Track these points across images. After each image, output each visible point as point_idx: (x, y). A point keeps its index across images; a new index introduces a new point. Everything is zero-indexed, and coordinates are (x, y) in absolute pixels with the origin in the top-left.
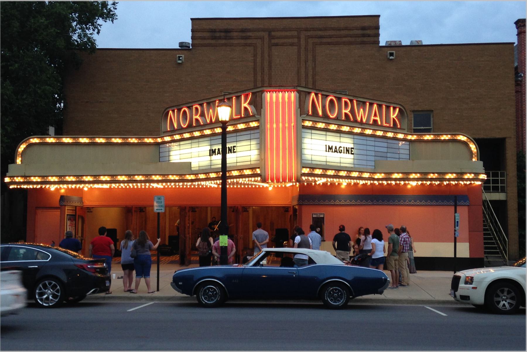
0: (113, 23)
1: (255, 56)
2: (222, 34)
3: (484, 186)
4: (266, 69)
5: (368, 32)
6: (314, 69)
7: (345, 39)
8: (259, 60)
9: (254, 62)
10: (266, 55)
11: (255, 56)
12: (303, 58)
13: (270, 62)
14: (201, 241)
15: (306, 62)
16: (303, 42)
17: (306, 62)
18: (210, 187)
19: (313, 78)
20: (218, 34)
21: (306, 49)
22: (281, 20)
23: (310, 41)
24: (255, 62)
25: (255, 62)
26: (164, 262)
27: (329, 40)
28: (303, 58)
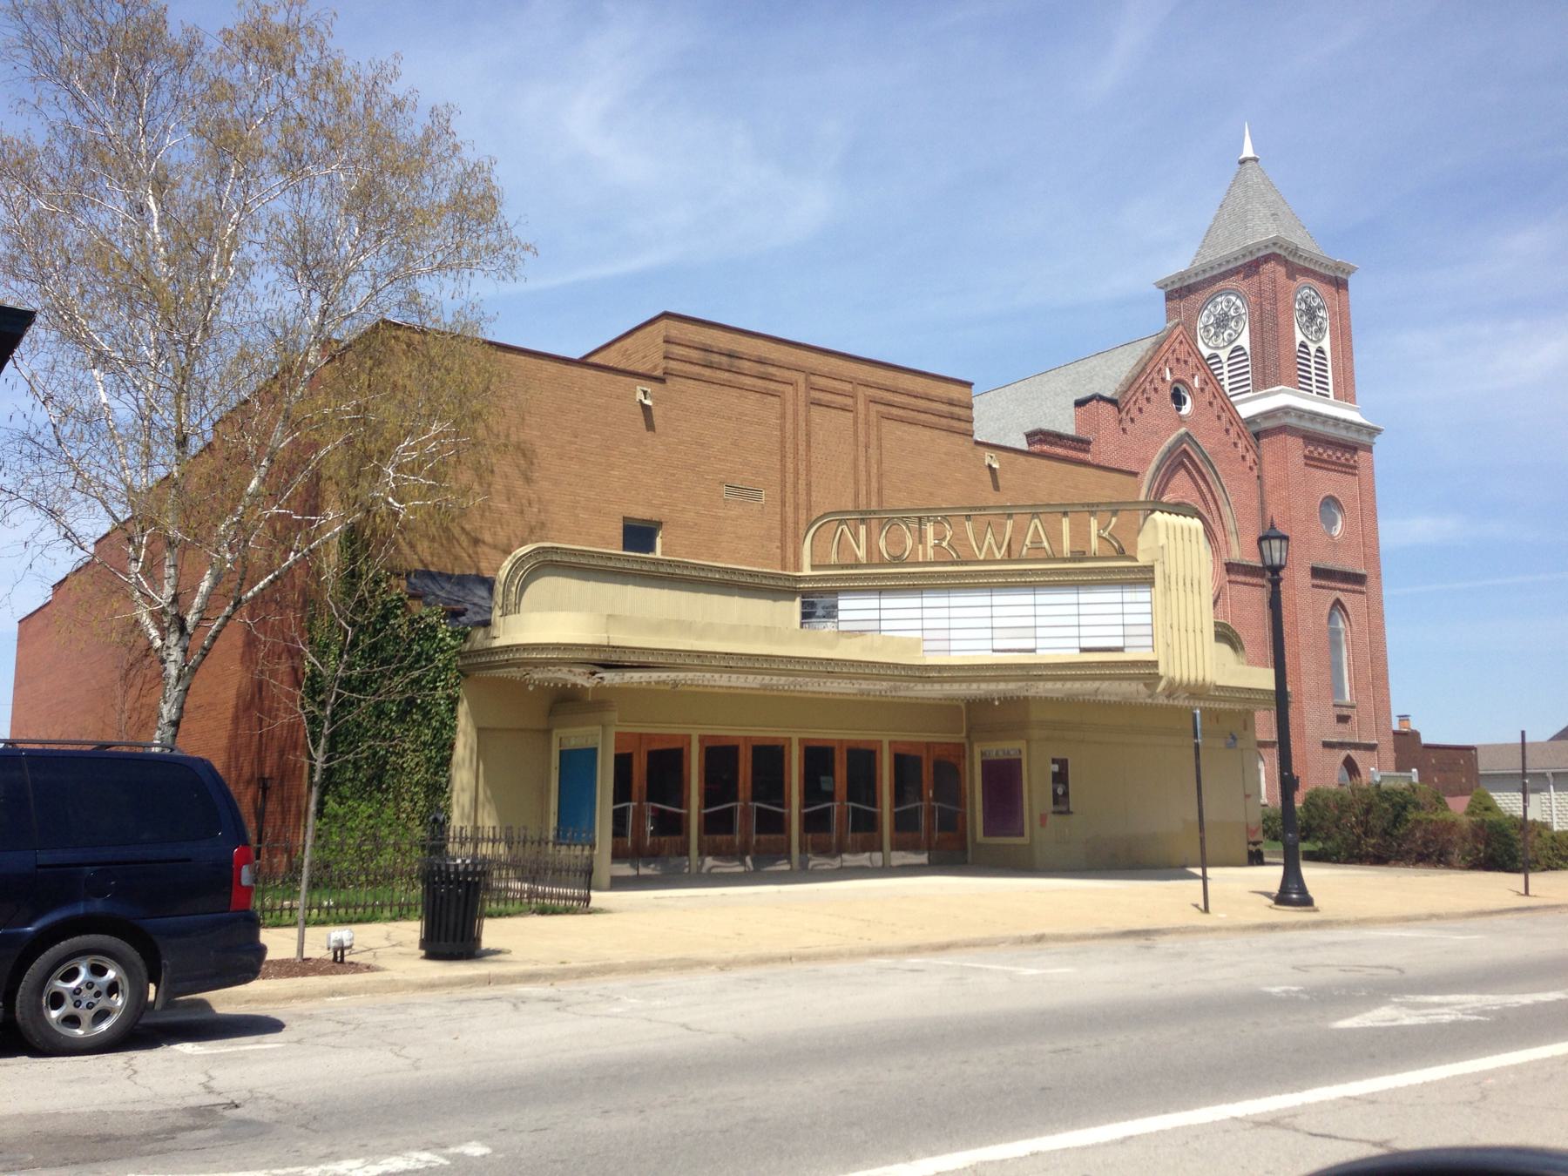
0: (1523, 733)
1: (783, 416)
2: (724, 359)
3: (689, 737)
4: (802, 448)
5: (956, 410)
6: (880, 462)
7: (923, 417)
8: (789, 426)
9: (781, 430)
10: (801, 419)
11: (783, 416)
12: (862, 438)
13: (808, 435)
14: (1490, 817)
15: (867, 447)
16: (861, 407)
17: (867, 447)
18: (574, 685)
19: (879, 482)
20: (716, 358)
21: (867, 423)
22: (1012, 455)
23: (874, 408)
24: (782, 429)
25: (782, 429)
26: (441, 905)
27: (901, 412)
28: (862, 438)
